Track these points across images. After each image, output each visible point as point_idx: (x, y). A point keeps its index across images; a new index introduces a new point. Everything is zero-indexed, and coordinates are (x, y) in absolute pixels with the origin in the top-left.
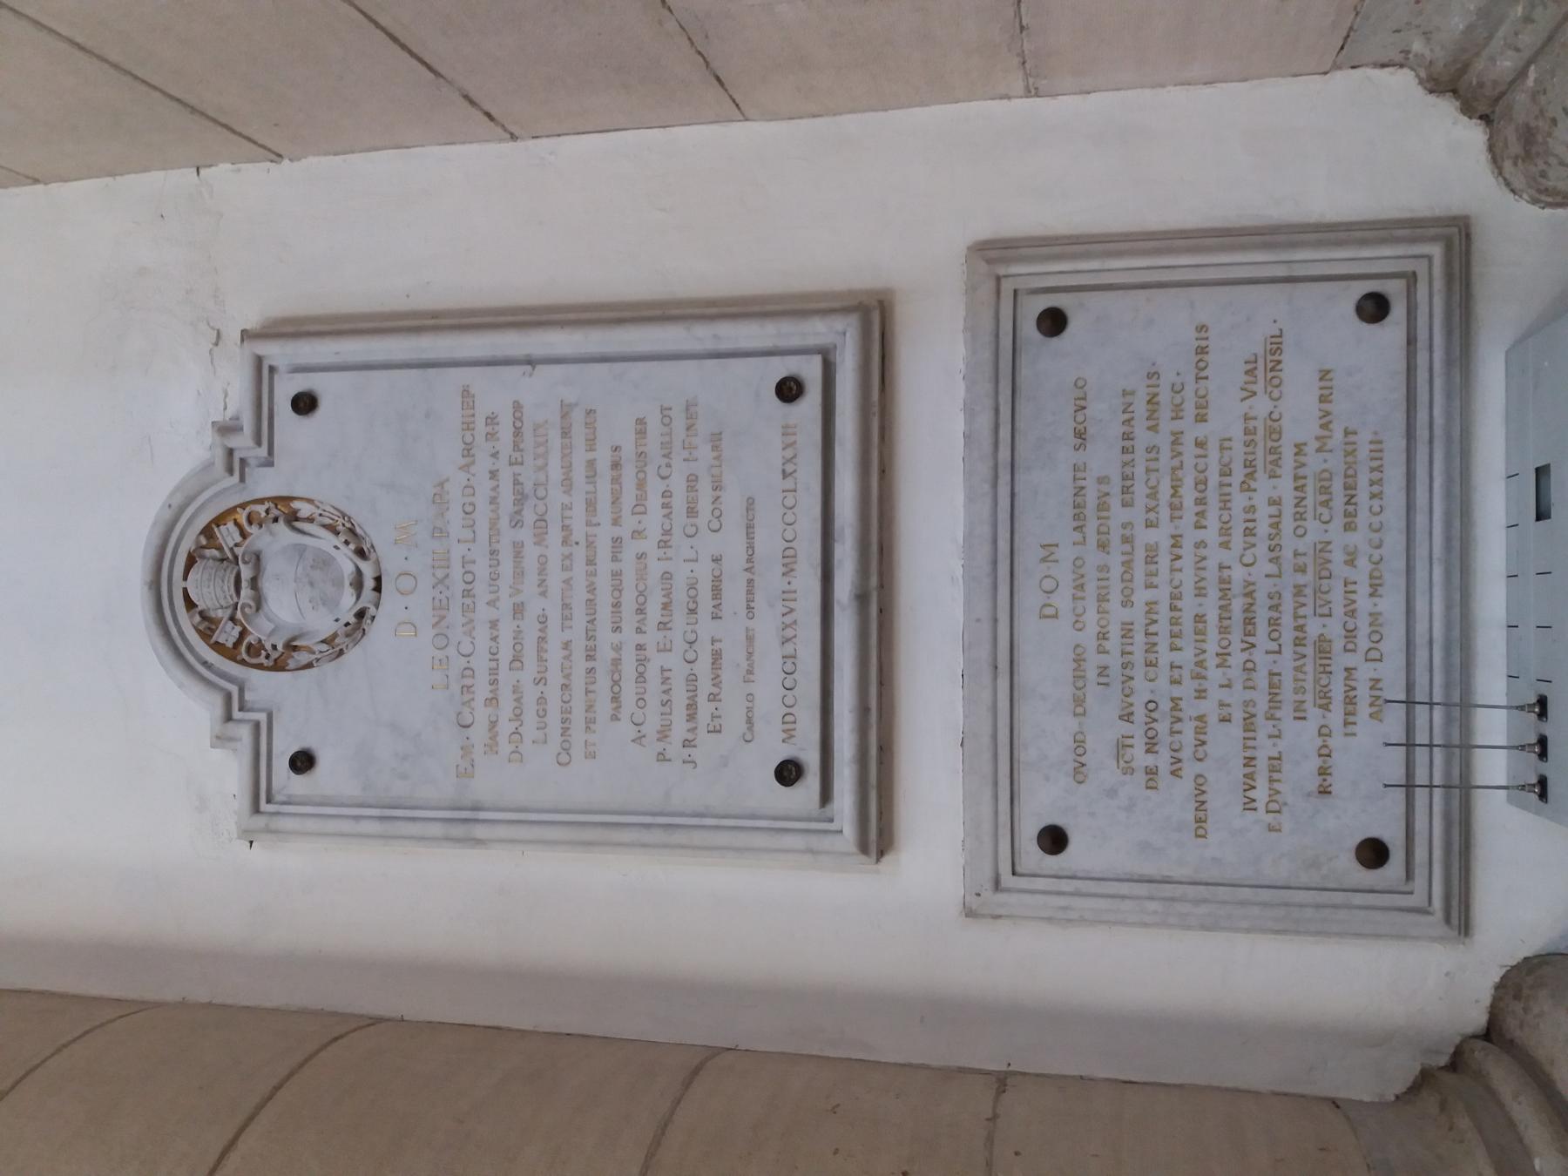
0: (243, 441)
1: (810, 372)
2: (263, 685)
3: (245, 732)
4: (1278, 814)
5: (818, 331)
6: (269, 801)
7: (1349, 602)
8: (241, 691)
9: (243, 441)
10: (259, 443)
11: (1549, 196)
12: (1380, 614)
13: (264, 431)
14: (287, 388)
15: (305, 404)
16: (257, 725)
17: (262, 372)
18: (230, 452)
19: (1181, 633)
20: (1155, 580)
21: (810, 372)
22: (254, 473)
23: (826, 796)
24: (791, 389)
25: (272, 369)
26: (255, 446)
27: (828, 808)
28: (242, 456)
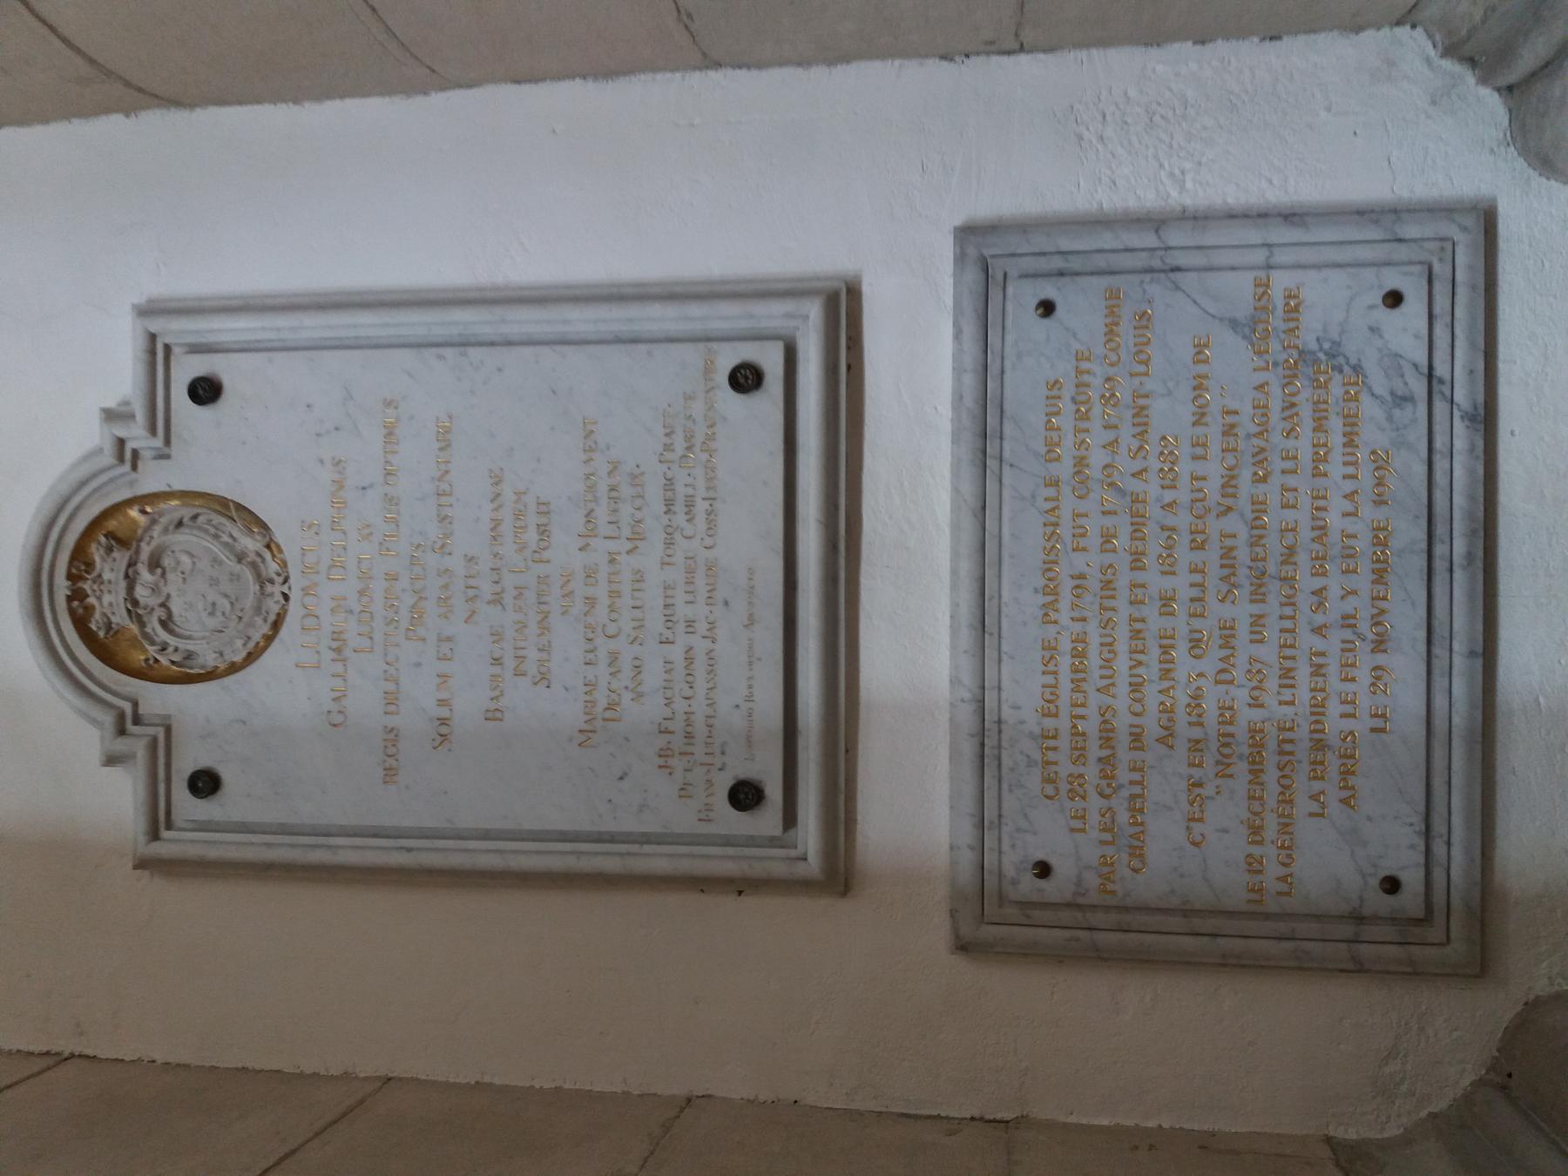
0: (136, 434)
1: (771, 360)
2: (158, 698)
3: (140, 748)
4: (1234, 539)
5: (772, 315)
6: (169, 827)
7: (1135, 663)
8: (135, 704)
9: (136, 434)
10: (153, 430)
11: (1545, 163)
12: (693, 713)
13: (159, 421)
14: (186, 370)
15: (206, 391)
16: (154, 740)
17: (156, 354)
18: (121, 443)
19: (550, 646)
20: (1352, 673)
21: (771, 360)
22: (147, 465)
23: (790, 818)
24: (746, 378)
25: (168, 349)
26: (149, 435)
27: (792, 832)
28: (134, 447)
